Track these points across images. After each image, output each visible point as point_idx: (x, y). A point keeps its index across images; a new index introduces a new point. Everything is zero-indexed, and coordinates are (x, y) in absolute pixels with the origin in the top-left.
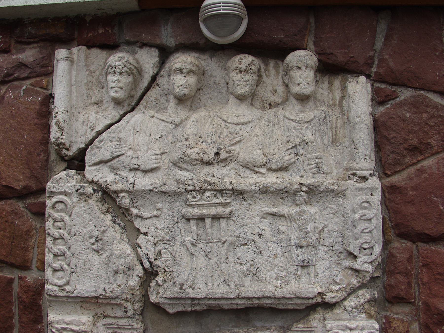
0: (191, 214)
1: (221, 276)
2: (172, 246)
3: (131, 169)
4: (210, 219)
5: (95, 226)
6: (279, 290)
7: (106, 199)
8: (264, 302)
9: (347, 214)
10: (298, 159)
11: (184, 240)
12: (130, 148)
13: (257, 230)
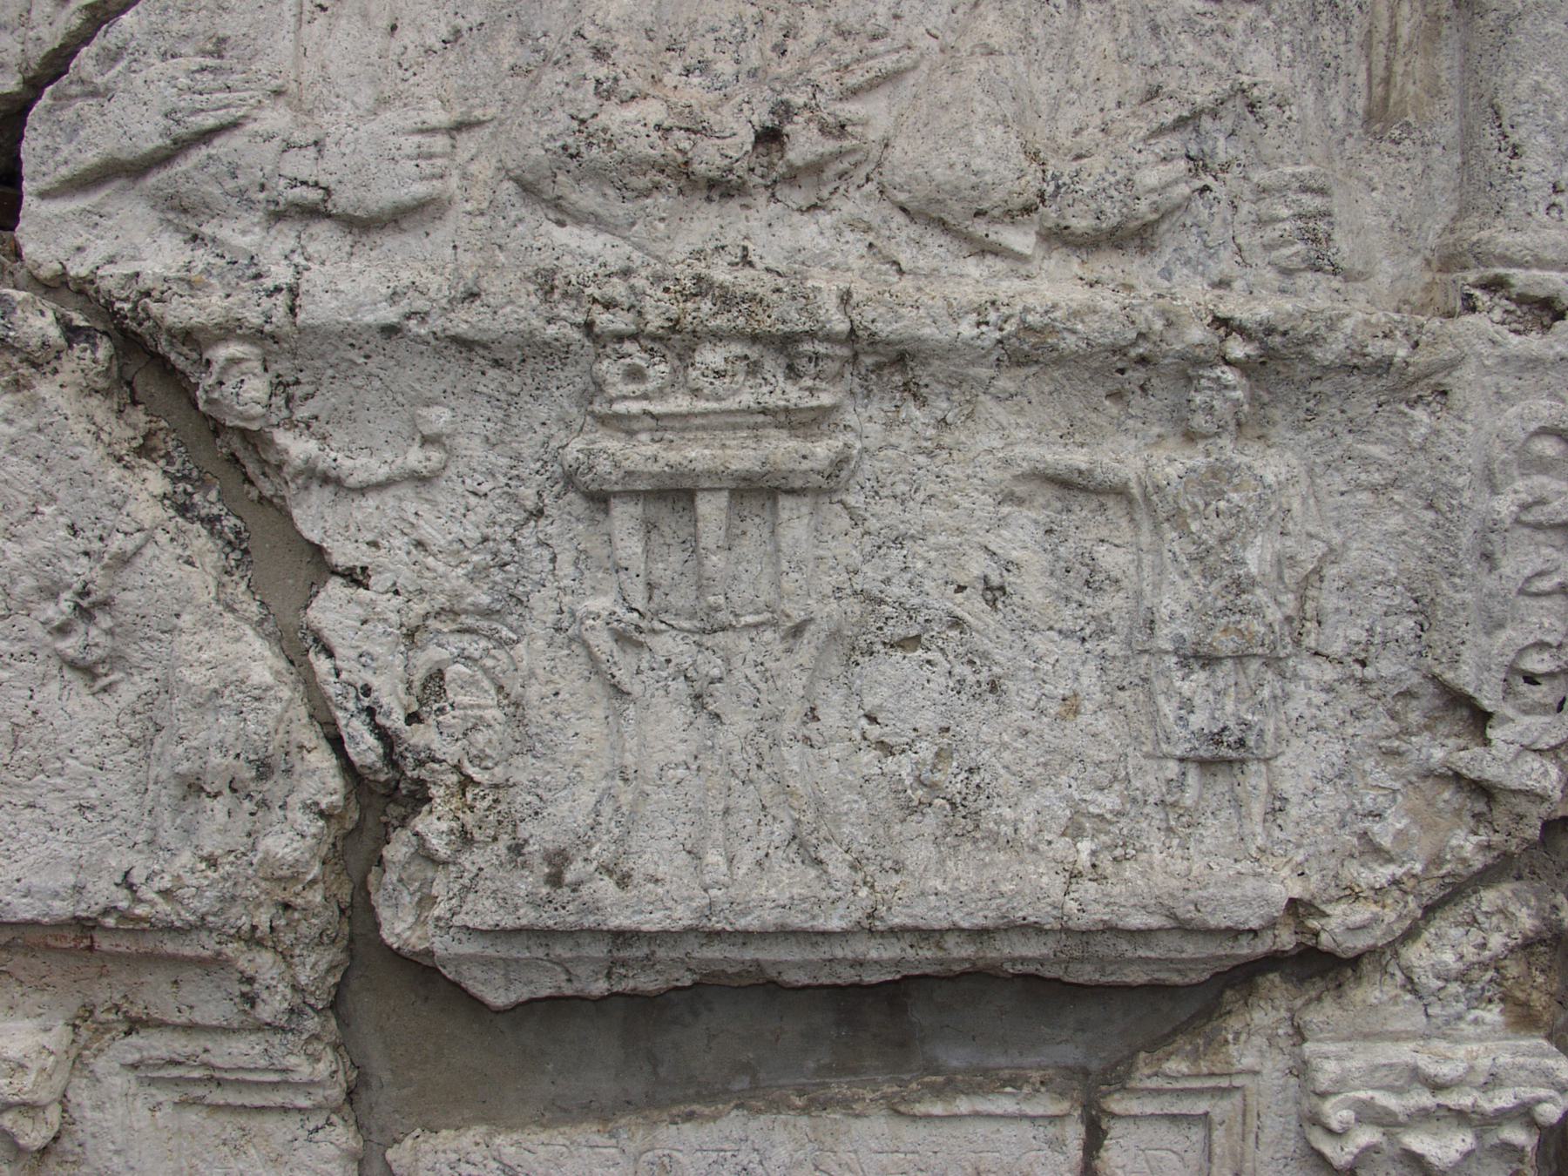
0: (616, 465)
1: (773, 811)
2: (502, 643)
3: (281, 207)
4: (722, 499)
5: (74, 530)
6: (1088, 889)
7: (139, 382)
8: (1007, 951)
9: (1456, 490)
10: (1206, 188)
11: (573, 614)
12: (278, 93)
13: (977, 566)
